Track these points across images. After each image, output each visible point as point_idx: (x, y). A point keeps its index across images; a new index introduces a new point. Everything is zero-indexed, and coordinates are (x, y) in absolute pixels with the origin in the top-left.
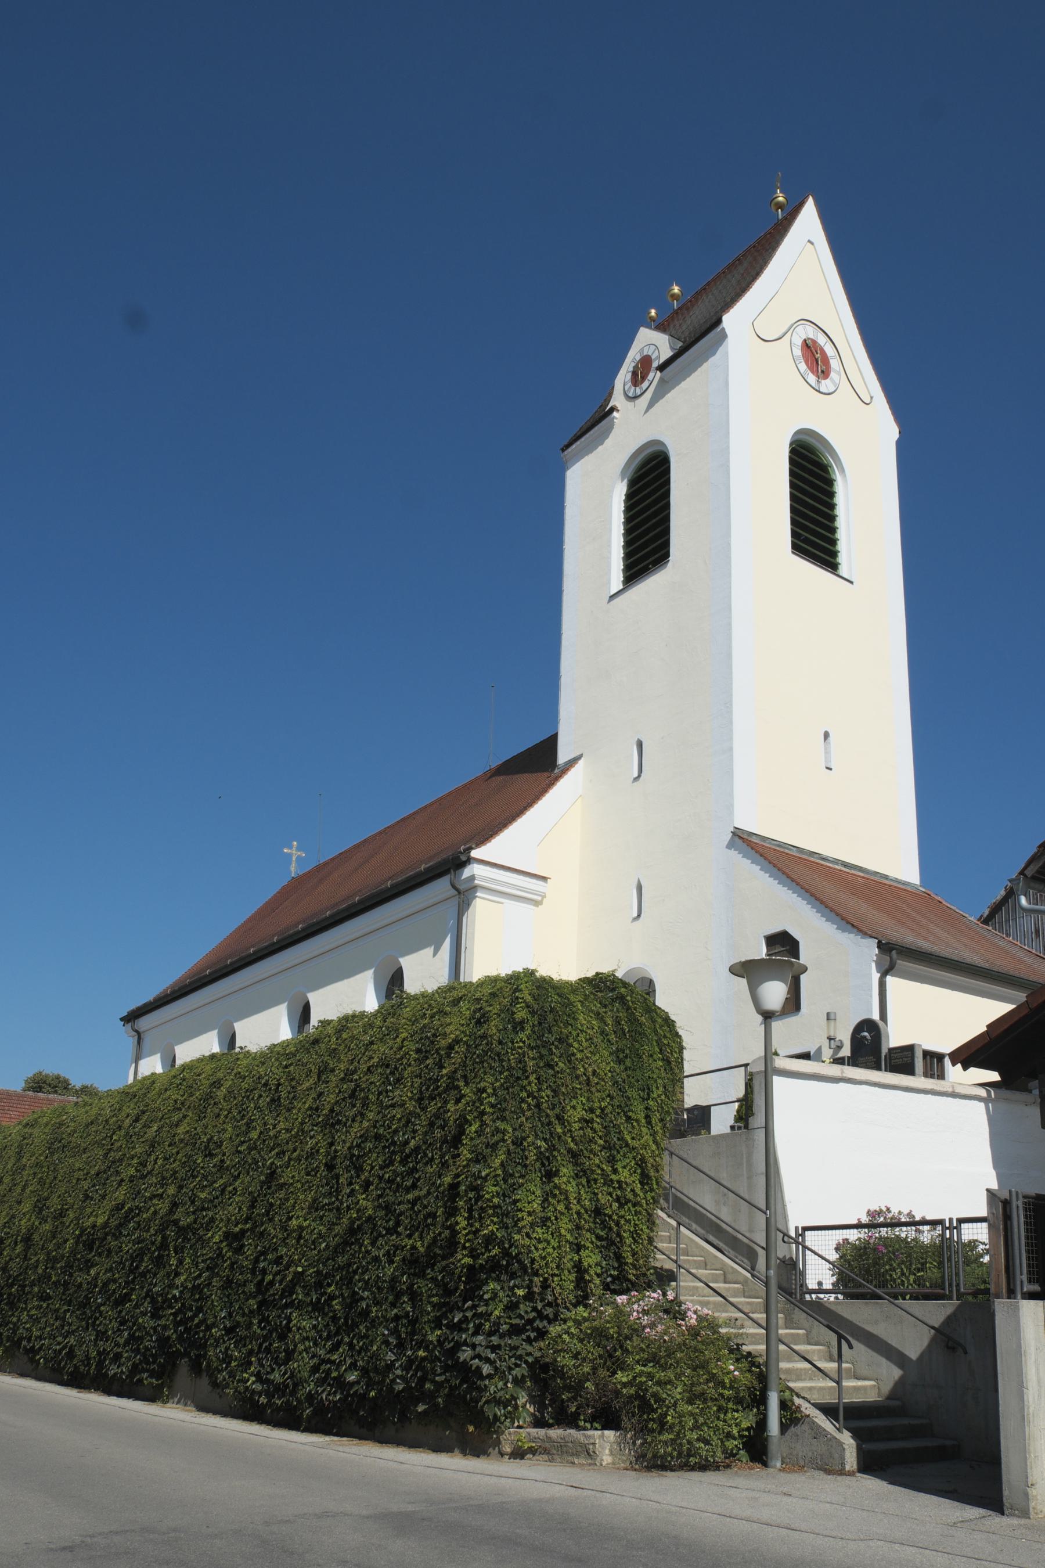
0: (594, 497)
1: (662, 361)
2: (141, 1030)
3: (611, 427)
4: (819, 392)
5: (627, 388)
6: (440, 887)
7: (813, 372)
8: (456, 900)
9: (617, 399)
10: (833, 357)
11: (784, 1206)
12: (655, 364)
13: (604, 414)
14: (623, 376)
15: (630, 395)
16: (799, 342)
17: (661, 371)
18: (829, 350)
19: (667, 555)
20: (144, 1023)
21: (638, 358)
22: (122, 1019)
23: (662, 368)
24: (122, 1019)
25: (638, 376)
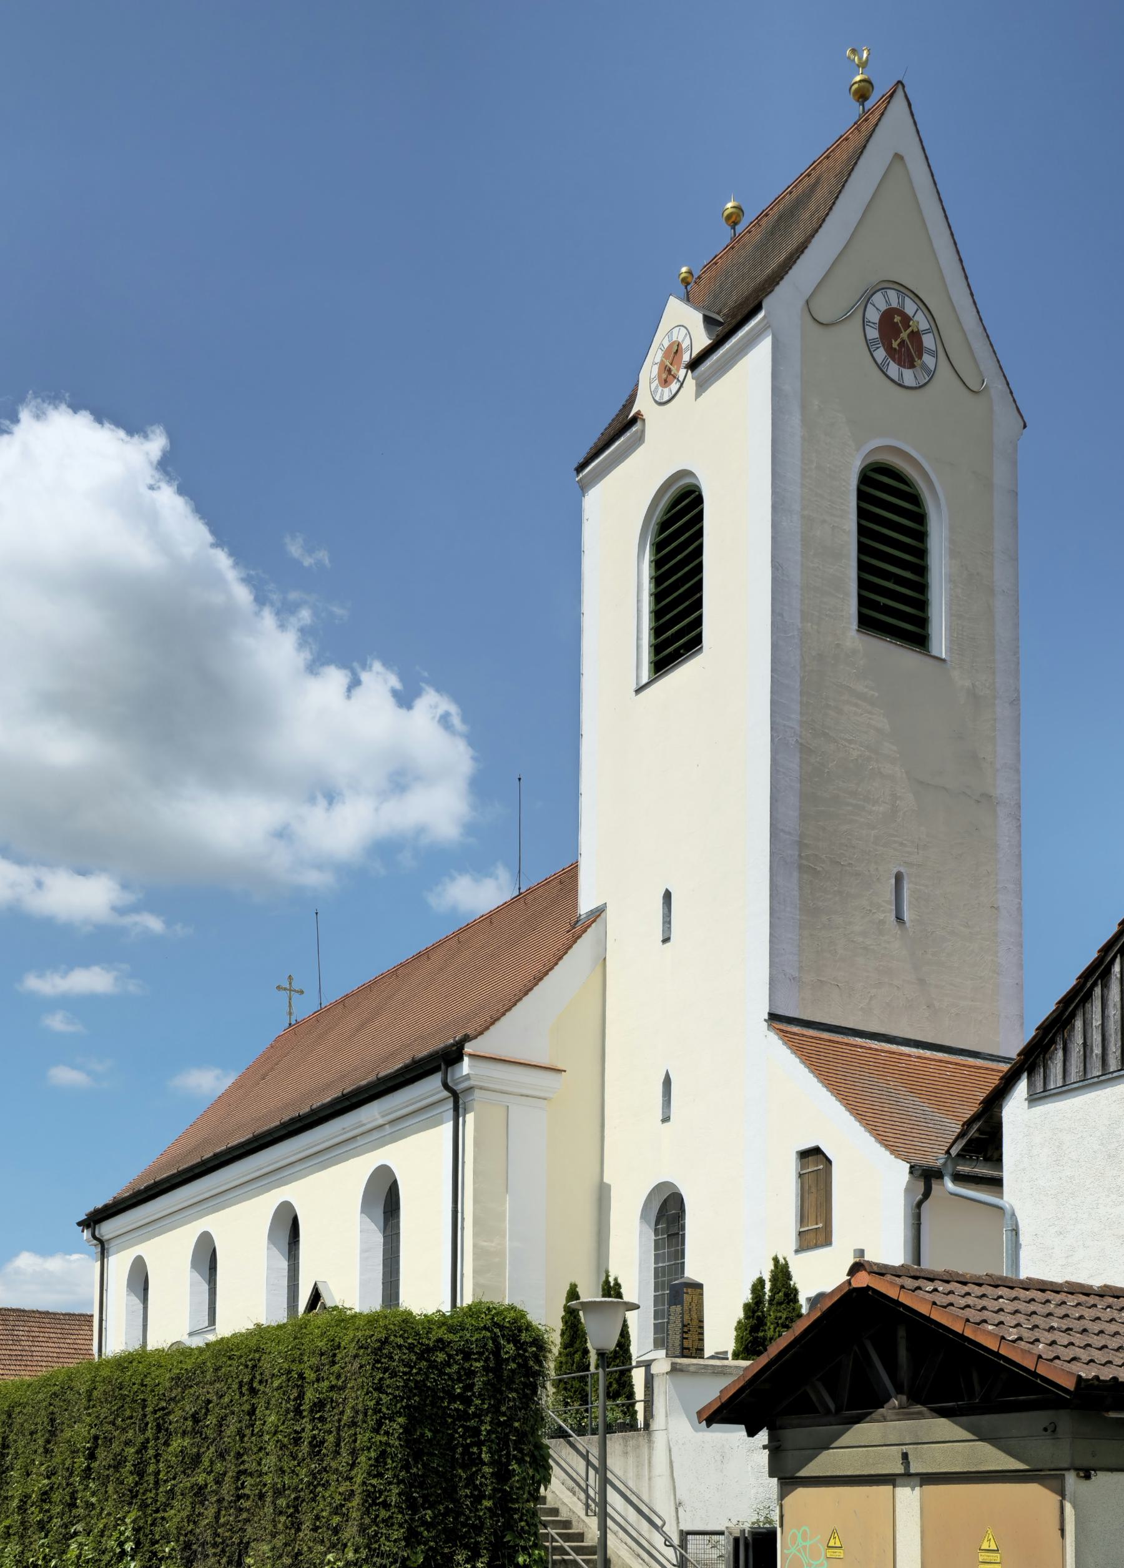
0: (456, 721)
1: (696, 351)
2: (105, 1238)
3: (640, 439)
4: (900, 385)
5: (653, 386)
6: (431, 1086)
7: (894, 361)
8: (450, 1105)
9: (643, 404)
10: (927, 331)
11: (1008, 1098)
12: (686, 358)
13: (625, 425)
14: (649, 371)
15: (657, 398)
16: (874, 316)
17: (692, 371)
18: (921, 322)
19: (697, 641)
20: (107, 1229)
21: (666, 344)
22: (79, 1224)
23: (693, 365)
24: (79, 1224)
25: (667, 375)
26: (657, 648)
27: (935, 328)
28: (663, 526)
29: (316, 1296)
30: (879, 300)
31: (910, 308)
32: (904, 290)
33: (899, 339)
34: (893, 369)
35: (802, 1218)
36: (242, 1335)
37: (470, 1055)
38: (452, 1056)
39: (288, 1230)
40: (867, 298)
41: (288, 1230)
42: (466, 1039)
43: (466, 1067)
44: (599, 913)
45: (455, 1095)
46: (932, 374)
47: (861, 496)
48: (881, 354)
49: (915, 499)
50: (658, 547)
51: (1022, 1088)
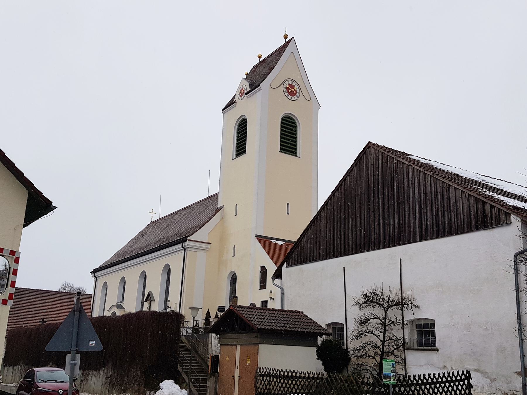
19: (245, 151)
20: (97, 274)
26: (237, 151)
27: (299, 88)
28: (239, 125)
29: (149, 295)
30: (287, 82)
31: (294, 84)
32: (293, 80)
33: (291, 91)
34: (290, 97)
35: (261, 283)
36: (132, 314)
37: (189, 240)
38: (185, 240)
39: (144, 277)
40: (284, 82)
41: (144, 277)
42: (188, 236)
43: (187, 243)
44: (222, 207)
45: (185, 249)
46: (298, 97)
47: (281, 122)
48: (287, 94)
49: (295, 123)
50: (238, 129)
51: (285, 265)
